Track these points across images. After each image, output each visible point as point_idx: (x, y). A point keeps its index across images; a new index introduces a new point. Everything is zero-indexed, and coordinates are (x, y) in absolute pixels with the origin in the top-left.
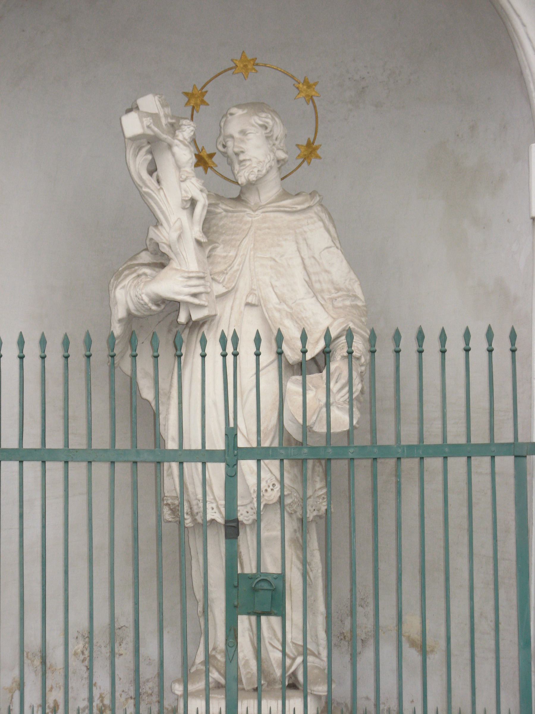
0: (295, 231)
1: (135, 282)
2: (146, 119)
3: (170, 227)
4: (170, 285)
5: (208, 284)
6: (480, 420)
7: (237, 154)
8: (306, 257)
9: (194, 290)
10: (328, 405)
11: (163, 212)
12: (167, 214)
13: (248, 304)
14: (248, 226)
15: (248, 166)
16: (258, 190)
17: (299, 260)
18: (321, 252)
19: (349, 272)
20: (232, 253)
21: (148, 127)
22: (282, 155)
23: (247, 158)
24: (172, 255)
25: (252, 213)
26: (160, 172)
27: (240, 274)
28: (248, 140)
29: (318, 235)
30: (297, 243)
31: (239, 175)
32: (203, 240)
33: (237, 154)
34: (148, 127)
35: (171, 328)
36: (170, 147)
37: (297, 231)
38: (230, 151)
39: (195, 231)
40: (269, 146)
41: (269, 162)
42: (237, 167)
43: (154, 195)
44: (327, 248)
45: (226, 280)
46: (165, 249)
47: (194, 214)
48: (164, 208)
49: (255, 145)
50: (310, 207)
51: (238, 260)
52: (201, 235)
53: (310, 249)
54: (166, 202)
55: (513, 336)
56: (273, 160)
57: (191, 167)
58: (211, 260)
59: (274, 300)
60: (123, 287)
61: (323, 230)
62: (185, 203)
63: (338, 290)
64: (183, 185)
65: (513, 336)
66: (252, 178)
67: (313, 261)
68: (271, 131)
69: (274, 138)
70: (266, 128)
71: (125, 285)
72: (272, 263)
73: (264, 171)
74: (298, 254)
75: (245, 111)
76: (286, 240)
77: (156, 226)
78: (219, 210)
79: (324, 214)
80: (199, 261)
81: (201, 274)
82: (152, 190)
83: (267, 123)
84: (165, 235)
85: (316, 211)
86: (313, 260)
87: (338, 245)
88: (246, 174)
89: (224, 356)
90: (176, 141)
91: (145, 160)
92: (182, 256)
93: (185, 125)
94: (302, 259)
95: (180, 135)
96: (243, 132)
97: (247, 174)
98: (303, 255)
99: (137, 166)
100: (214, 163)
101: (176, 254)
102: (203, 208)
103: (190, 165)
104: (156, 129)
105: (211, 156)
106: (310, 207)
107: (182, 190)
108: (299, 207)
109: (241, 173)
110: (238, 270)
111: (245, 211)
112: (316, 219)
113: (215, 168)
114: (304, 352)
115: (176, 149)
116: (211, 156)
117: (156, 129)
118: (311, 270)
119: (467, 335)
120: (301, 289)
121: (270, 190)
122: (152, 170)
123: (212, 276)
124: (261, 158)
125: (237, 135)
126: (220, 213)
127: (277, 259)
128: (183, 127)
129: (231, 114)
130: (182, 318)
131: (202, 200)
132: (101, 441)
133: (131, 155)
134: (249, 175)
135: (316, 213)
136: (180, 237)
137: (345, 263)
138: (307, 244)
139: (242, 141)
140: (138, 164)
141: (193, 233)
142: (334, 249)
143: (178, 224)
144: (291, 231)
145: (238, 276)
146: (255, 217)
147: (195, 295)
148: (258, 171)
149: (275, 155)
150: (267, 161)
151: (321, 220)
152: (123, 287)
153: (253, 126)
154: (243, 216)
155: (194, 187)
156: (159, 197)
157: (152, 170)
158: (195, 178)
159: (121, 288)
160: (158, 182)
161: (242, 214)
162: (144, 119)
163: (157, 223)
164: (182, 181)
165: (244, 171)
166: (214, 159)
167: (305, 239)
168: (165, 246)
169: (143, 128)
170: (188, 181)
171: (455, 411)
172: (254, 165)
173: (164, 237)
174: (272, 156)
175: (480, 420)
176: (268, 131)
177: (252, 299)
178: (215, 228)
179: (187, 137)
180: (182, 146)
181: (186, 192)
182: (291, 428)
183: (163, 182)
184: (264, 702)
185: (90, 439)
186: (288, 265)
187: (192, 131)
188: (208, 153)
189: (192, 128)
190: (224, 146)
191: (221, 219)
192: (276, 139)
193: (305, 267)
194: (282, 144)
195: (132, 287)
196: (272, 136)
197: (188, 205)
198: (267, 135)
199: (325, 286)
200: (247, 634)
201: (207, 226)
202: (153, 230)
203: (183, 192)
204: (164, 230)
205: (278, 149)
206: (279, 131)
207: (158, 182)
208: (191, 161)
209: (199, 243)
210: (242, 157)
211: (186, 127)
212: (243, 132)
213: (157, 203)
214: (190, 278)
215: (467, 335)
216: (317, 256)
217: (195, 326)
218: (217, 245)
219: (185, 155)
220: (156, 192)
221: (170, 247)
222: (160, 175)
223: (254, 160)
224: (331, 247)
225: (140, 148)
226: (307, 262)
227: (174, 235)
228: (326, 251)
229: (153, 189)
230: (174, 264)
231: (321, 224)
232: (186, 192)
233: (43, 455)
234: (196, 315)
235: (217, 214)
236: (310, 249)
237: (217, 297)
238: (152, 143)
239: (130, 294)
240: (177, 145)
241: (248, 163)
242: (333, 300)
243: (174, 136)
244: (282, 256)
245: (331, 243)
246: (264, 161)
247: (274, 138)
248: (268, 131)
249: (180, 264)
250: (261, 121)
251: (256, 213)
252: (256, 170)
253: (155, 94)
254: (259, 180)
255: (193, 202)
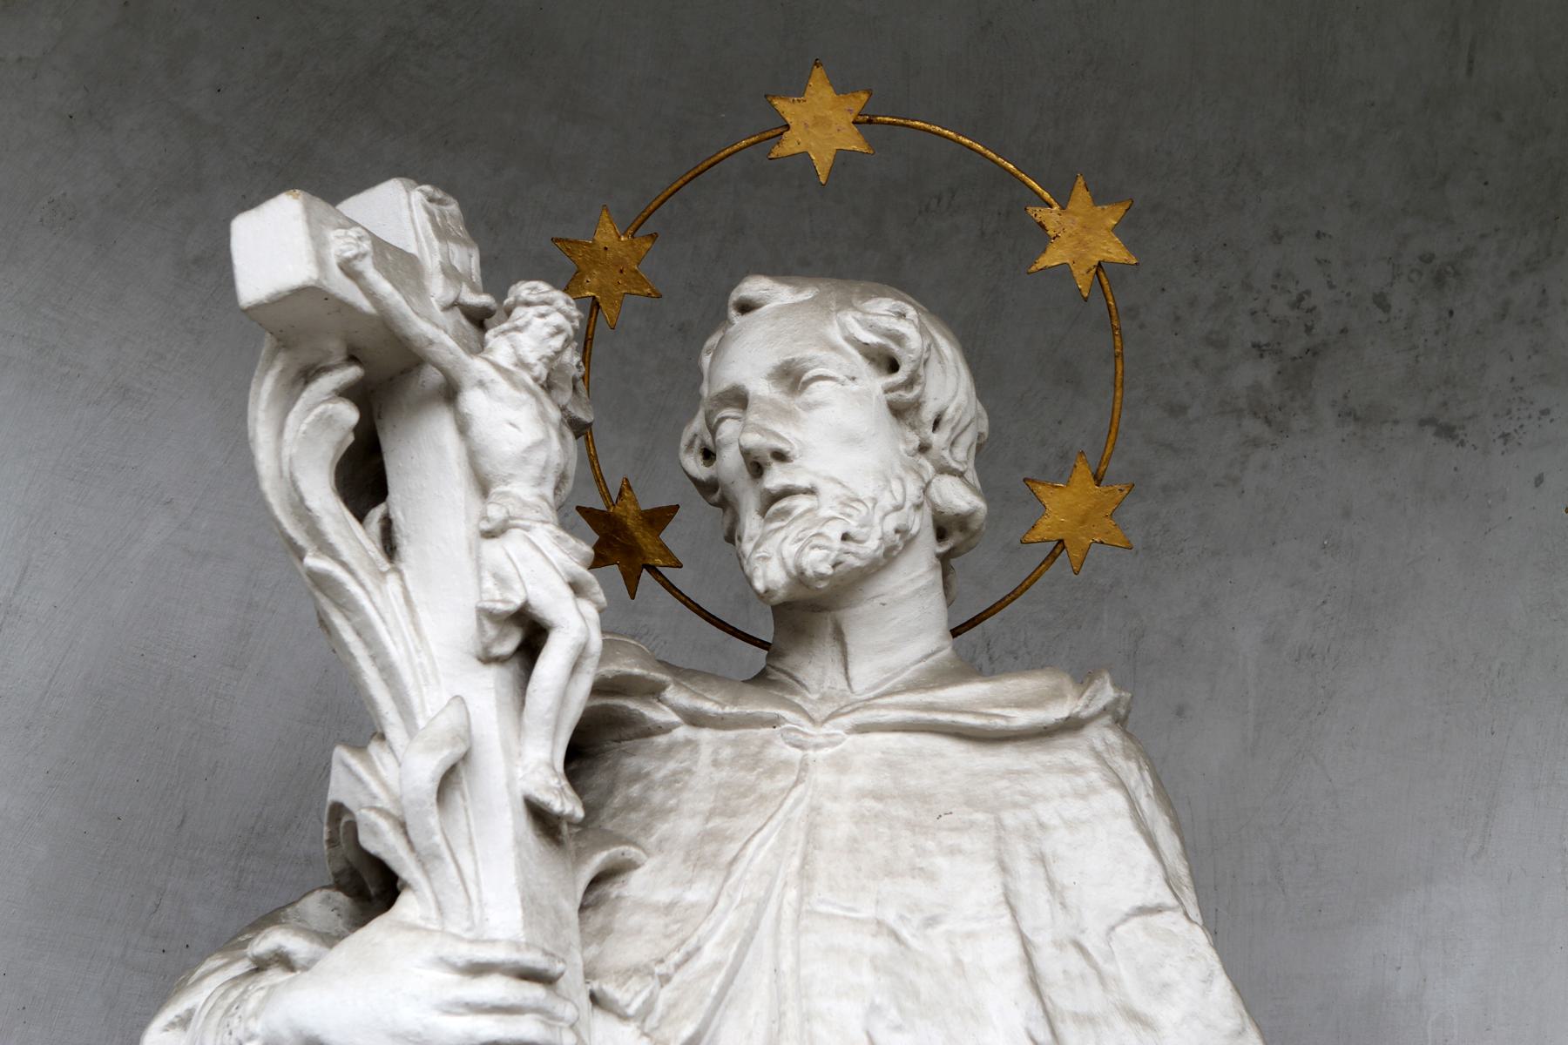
0: (999, 820)
1: (235, 994)
2: (341, 232)
3: (411, 729)
5: (568, 1012)
8: (1042, 941)
11: (388, 672)
12: (407, 677)
14: (783, 781)
15: (801, 515)
16: (839, 635)
17: (1011, 948)
18: (1113, 928)
19: (1241, 1033)
20: (698, 893)
21: (349, 269)
22: (959, 497)
23: (802, 481)
24: (407, 869)
25: (807, 727)
26: (398, 501)
27: (724, 989)
28: (809, 407)
30: (1004, 868)
31: (761, 552)
32: (565, 804)
33: (756, 468)
34: (349, 269)
36: (450, 393)
37: (1009, 819)
39: (536, 765)
40: (902, 447)
41: (898, 508)
42: (751, 524)
43: (353, 587)
44: (1143, 911)
45: (660, 1007)
46: (383, 841)
47: (530, 688)
48: (396, 653)
49: (839, 417)
50: (1072, 726)
52: (558, 781)
53: (1064, 906)
54: (407, 629)
56: (918, 507)
57: (540, 481)
58: (597, 919)
60: (184, 1022)
61: (1126, 825)
62: (491, 631)
64: (492, 549)
66: (817, 562)
67: (1074, 960)
68: (910, 383)
69: (928, 414)
70: (893, 366)
71: (191, 1012)
72: (883, 945)
73: (872, 546)
74: (1007, 920)
75: (807, 294)
76: (953, 851)
77: (359, 747)
78: (658, 714)
79: (1133, 765)
80: (531, 904)
81: (533, 959)
82: (344, 565)
83: (899, 339)
85: (1100, 746)
86: (1073, 956)
87: (1194, 912)
88: (790, 549)
90: (478, 365)
91: (327, 421)
92: (452, 869)
93: (528, 304)
94: (1025, 943)
95: (500, 346)
96: (792, 377)
97: (795, 548)
98: (1026, 928)
99: (286, 452)
100: (666, 553)
101: (426, 860)
102: (575, 667)
103: (533, 471)
104: (384, 287)
105: (660, 518)
106: (1072, 726)
107: (486, 575)
108: (1022, 718)
109: (769, 548)
110: (717, 966)
111: (774, 722)
112: (1094, 776)
113: (666, 572)
115: (473, 401)
116: (660, 518)
117: (384, 287)
118: (1063, 1000)
121: (902, 626)
122: (364, 478)
123: (595, 985)
124: (865, 488)
125: (760, 387)
126: (666, 729)
127: (905, 933)
128: (519, 312)
129: (746, 307)
131: (574, 625)
133: (263, 404)
134: (801, 550)
135: (1098, 756)
136: (448, 781)
137: (1222, 986)
138: (1051, 884)
139: (787, 414)
140: (296, 440)
141: (520, 773)
142: (1172, 921)
143: (449, 720)
144: (980, 817)
145: (714, 990)
146: (817, 746)
148: (845, 537)
149: (925, 490)
150: (887, 502)
151: (1122, 786)
152: (184, 1022)
153: (835, 348)
154: (767, 742)
155: (544, 566)
156: (378, 598)
157: (364, 478)
158: (551, 527)
159: (172, 1025)
160: (389, 546)
161: (765, 731)
162: (332, 234)
163: (363, 730)
164: (489, 535)
165: (781, 535)
166: (669, 536)
167: (1042, 859)
168: (384, 825)
169: (321, 263)
170: (515, 534)
172: (825, 512)
173: (384, 785)
174: (913, 490)
176: (900, 377)
178: (635, 790)
179: (532, 358)
180: (503, 386)
181: (502, 581)
183: (406, 549)
186: (958, 962)
187: (559, 330)
188: (646, 505)
189: (557, 319)
190: (709, 455)
191: (670, 750)
192: (936, 424)
193: (1035, 982)
194: (960, 453)
195: (219, 1013)
196: (917, 405)
197: (509, 645)
198: (892, 396)
201: (592, 746)
202: (347, 767)
203: (489, 583)
204: (388, 759)
205: (944, 470)
207: (389, 546)
208: (540, 456)
209: (542, 818)
210: (776, 478)
211: (531, 311)
212: (792, 377)
213: (365, 631)
214: (478, 969)
216: (1092, 942)
218: (632, 852)
220: (362, 574)
221: (402, 826)
222: (398, 516)
223: (828, 490)
224: (1158, 909)
225: (308, 375)
226: (1050, 962)
227: (424, 768)
228: (1135, 922)
229: (354, 564)
231: (1118, 800)
232: (502, 581)
235: (650, 731)
236: (1064, 906)
240: (481, 384)
241: (801, 503)
243: (479, 348)
244: (932, 921)
245: (1159, 893)
246: (875, 501)
247: (928, 414)
248: (900, 377)
249: (440, 910)
250: (872, 328)
251: (828, 728)
252: (834, 531)
255: (531, 634)
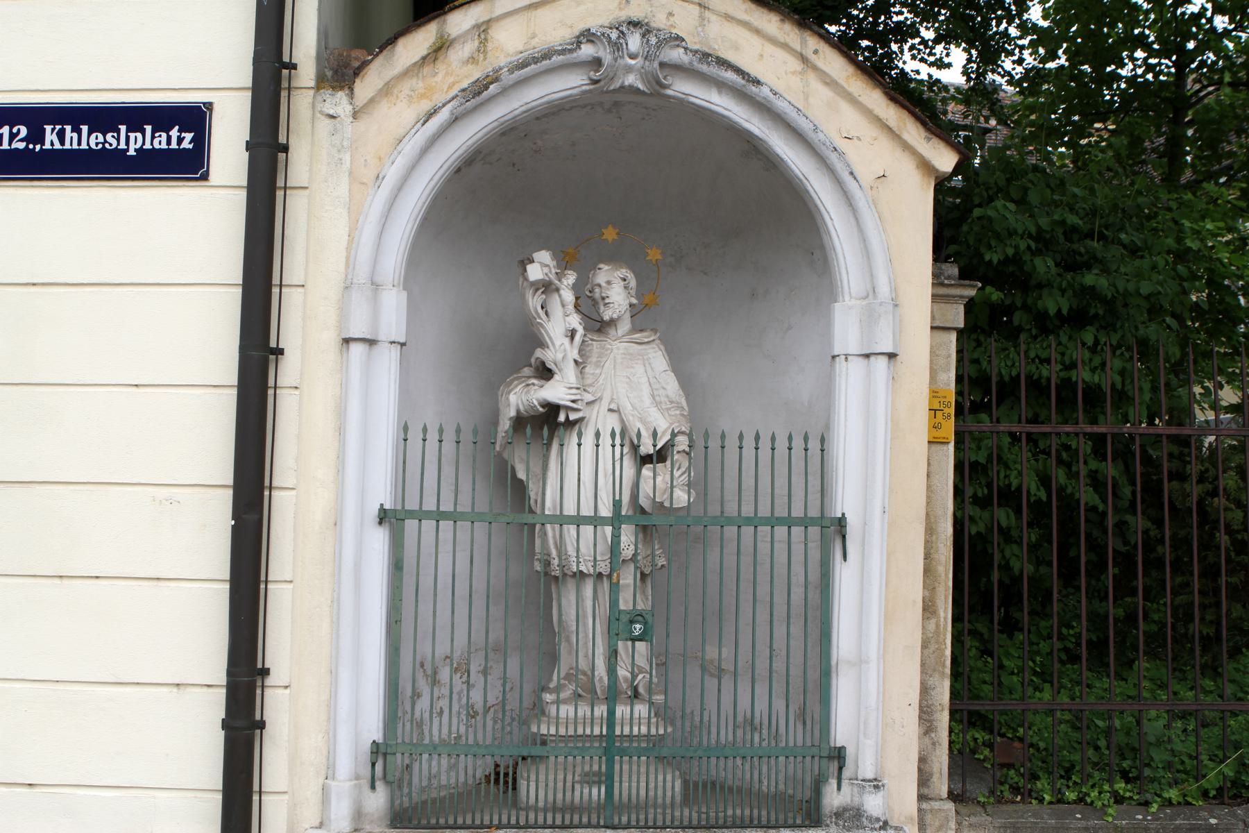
4: (555, 392)
6: (781, 503)
7: (603, 299)
9: (574, 398)
10: (672, 487)
11: (550, 338)
13: (610, 410)
20: (598, 371)
22: (634, 301)
29: (658, 359)
33: (603, 299)
35: (549, 423)
36: (557, 290)
38: (597, 295)
39: (574, 354)
42: (602, 308)
49: (617, 290)
51: (603, 376)
55: (823, 440)
59: (629, 407)
63: (672, 402)
65: (823, 440)
66: (615, 316)
84: (548, 356)
89: (613, 446)
96: (609, 283)
114: (655, 446)
115: (562, 292)
119: (741, 437)
120: (647, 400)
121: (625, 326)
125: (603, 284)
130: (562, 418)
132: (465, 506)
147: (573, 401)
155: (575, 321)
163: (542, 345)
171: (748, 496)
175: (781, 503)
177: (613, 406)
182: (643, 501)
184: (596, 709)
185: (455, 505)
199: (663, 399)
200: (601, 658)
206: (633, 283)
209: (576, 361)
212: (609, 283)
215: (741, 437)
217: (570, 424)
219: (569, 296)
225: (537, 290)
227: (560, 356)
230: (556, 377)
233: (439, 516)
234: (573, 417)
237: (587, 403)
238: (547, 287)
239: (523, 396)
242: (668, 409)
253: (548, 249)
254: (619, 318)
